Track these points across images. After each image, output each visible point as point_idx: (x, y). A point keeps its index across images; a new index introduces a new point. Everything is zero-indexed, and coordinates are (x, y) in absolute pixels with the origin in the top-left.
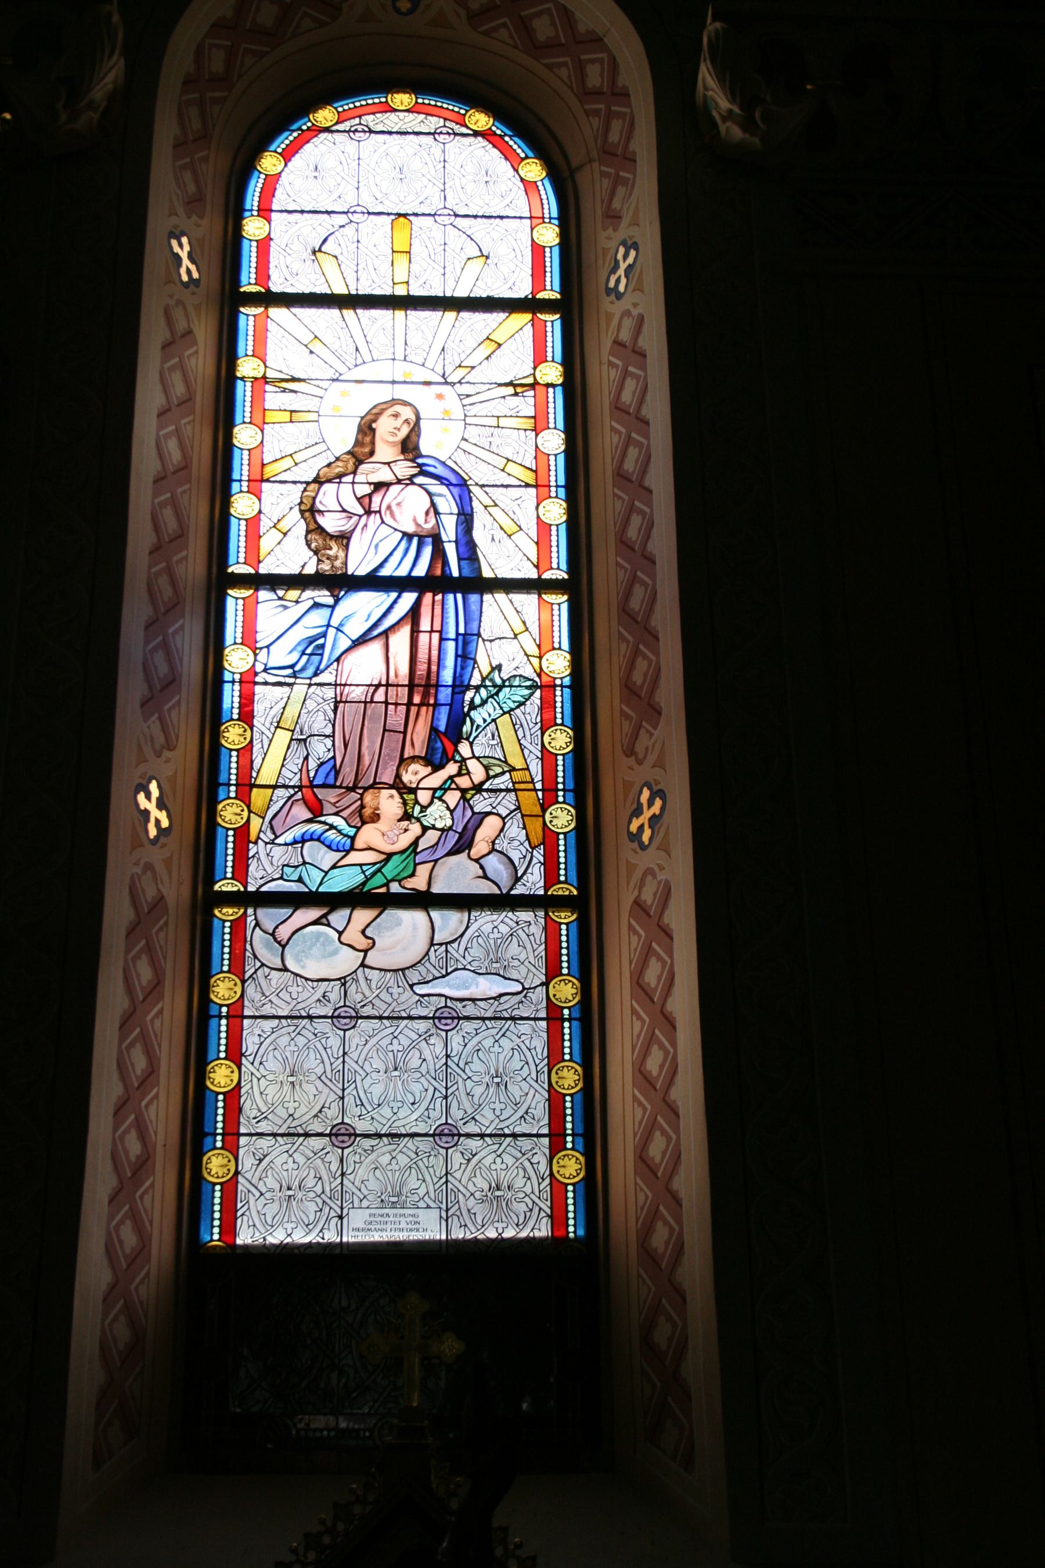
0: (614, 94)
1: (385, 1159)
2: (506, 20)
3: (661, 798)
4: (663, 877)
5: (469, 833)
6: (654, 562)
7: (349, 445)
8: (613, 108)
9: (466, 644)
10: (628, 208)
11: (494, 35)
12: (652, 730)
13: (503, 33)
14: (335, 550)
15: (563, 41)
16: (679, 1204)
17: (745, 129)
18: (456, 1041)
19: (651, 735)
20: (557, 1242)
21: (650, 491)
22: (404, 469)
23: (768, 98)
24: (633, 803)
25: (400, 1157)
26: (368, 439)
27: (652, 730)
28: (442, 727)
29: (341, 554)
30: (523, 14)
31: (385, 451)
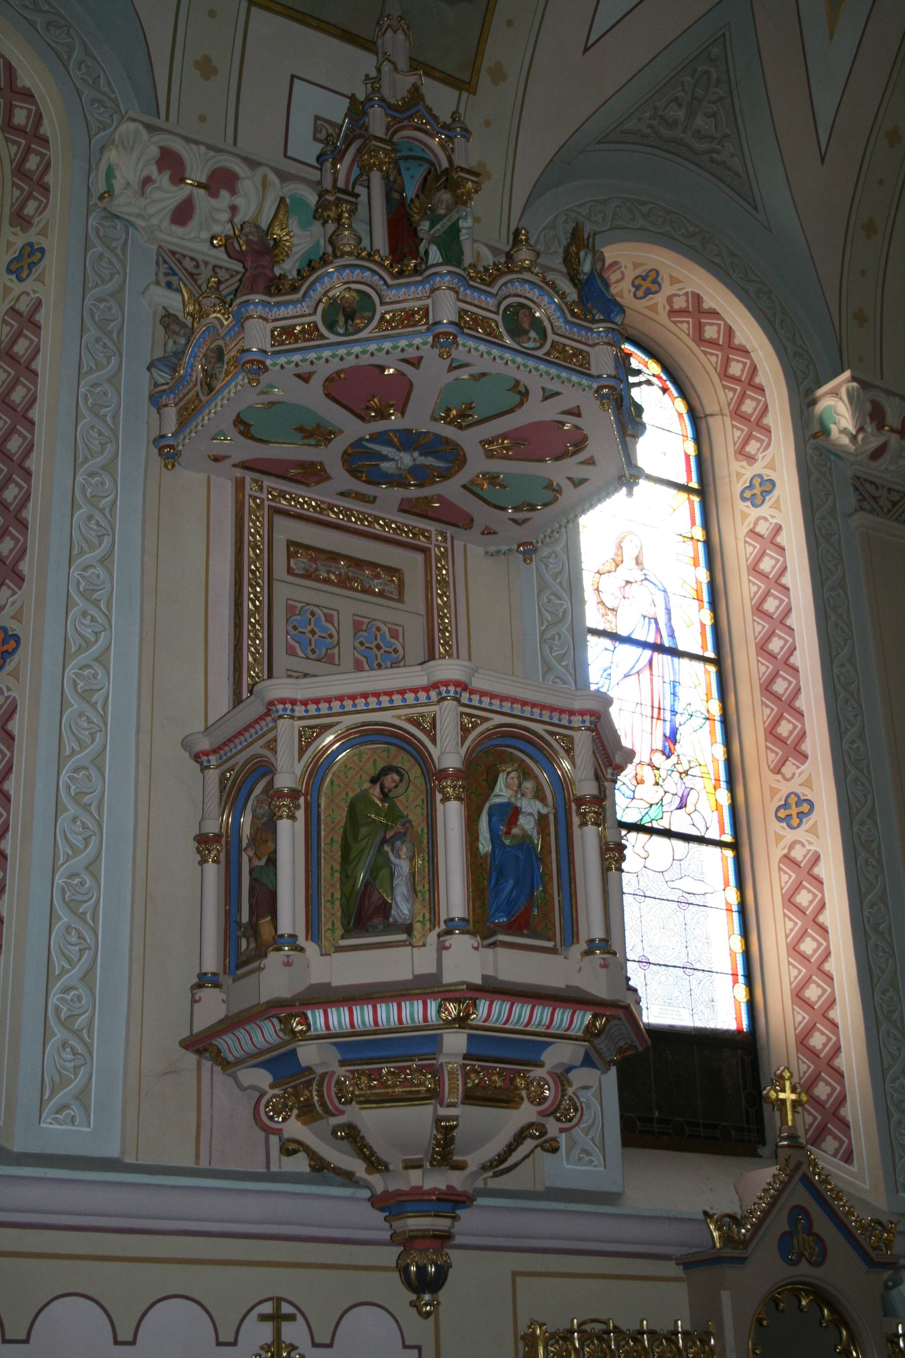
0: (38, 184)
1: (663, 978)
2: (690, 320)
3: (16, 641)
4: (813, 848)
5: (684, 800)
6: (798, 671)
7: (612, 555)
8: (34, 193)
9: (674, 687)
10: (39, 222)
11: (679, 325)
12: (17, 590)
13: (685, 326)
14: (611, 616)
15: (721, 343)
16: (836, 1026)
17: (851, 441)
18: (688, 915)
19: (14, 593)
20: (740, 1031)
21: (793, 630)
22: (637, 575)
23: (869, 430)
24: (780, 800)
25: (670, 978)
26: (620, 552)
27: (17, 590)
28: (668, 735)
29: (613, 620)
30: (702, 320)
31: (629, 561)
